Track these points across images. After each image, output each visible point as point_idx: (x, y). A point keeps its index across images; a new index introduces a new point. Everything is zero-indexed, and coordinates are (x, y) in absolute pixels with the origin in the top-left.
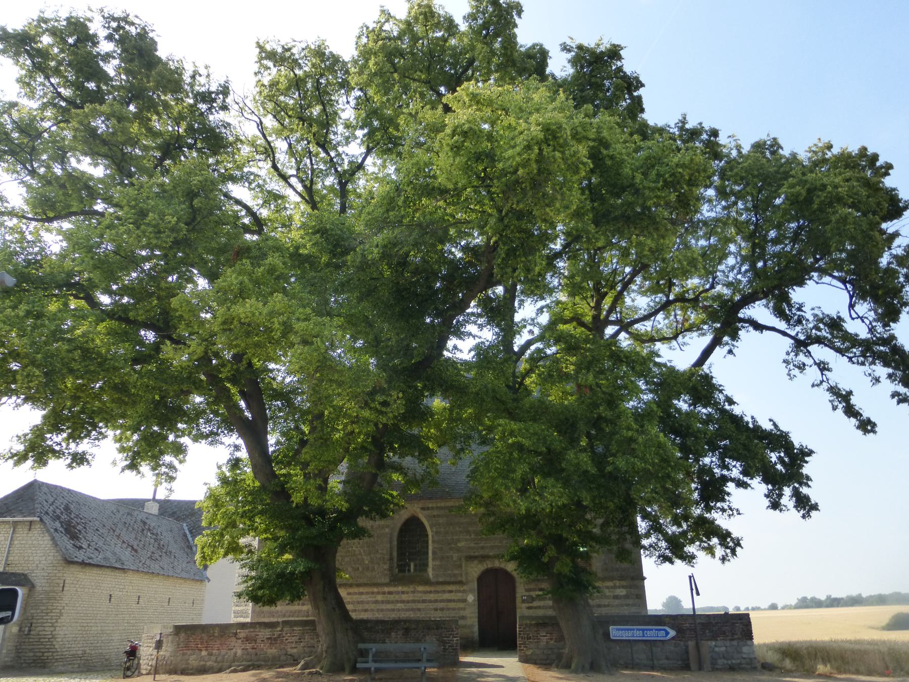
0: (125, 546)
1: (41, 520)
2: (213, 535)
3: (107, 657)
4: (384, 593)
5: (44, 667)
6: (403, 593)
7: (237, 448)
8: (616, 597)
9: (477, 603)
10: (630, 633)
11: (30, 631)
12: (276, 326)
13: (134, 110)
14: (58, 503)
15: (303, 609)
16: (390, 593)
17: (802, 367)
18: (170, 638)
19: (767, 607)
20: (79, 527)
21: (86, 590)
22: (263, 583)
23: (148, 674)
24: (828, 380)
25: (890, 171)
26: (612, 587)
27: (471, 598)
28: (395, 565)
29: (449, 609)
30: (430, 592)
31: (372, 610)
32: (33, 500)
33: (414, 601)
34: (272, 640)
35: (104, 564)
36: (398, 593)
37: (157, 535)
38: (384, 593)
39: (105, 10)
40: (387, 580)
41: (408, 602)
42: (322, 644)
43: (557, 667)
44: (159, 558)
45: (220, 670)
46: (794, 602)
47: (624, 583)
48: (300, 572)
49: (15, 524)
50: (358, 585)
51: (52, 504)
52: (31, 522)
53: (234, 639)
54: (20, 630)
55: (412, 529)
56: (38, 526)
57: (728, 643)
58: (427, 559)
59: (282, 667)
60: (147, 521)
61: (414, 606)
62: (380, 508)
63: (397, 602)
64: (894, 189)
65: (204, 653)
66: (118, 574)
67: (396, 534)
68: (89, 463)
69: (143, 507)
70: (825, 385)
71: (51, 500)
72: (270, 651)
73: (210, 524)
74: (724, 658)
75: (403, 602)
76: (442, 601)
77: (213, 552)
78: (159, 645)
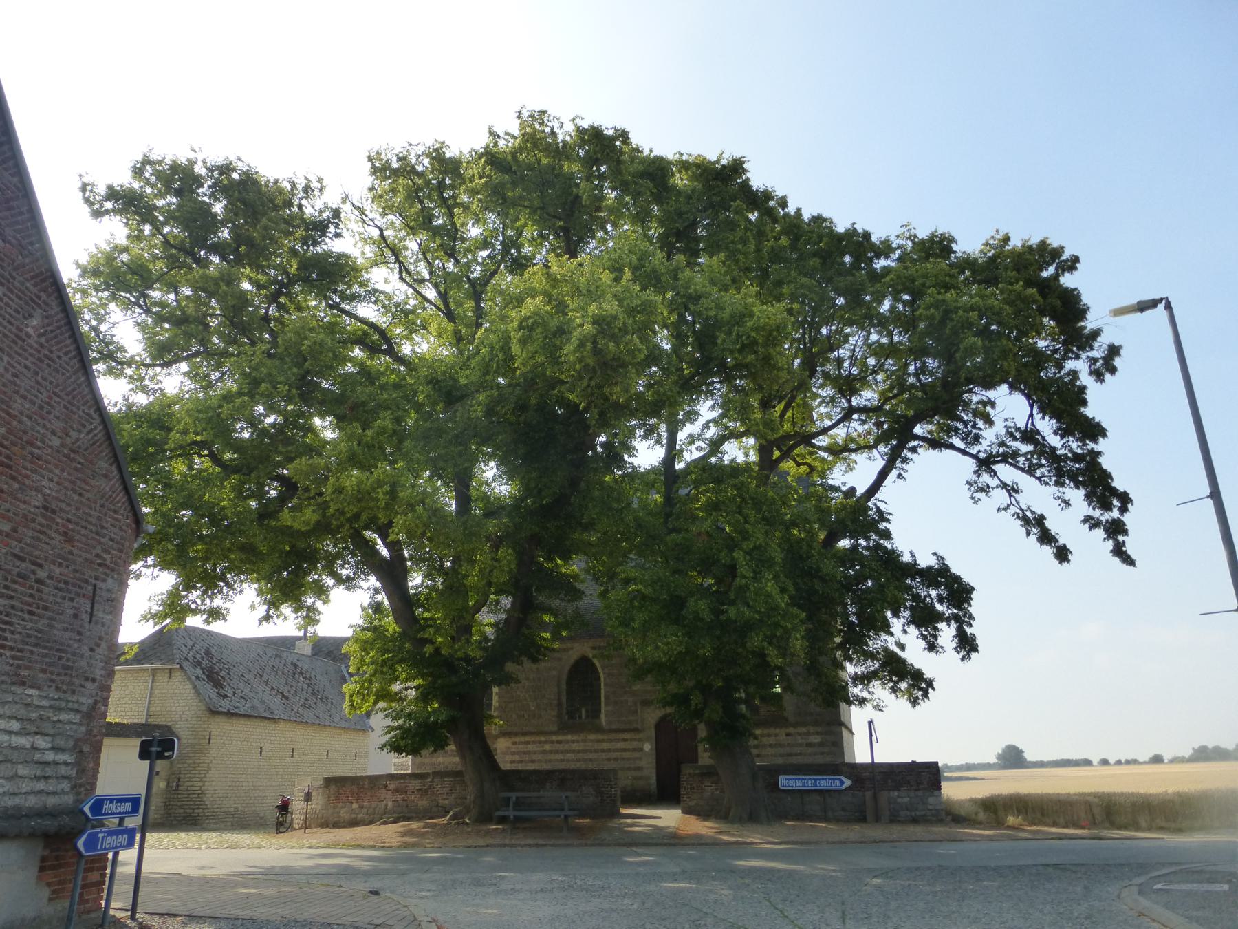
1: (181, 667)
2: (363, 682)
3: (262, 815)
4: (552, 742)
5: (196, 825)
6: (573, 742)
7: (377, 591)
8: (810, 745)
9: (654, 752)
11: (178, 786)
12: (381, 496)
13: (226, 458)
14: (197, 647)
15: (448, 758)
16: (559, 742)
17: (985, 489)
18: (321, 790)
19: (1147, 759)
22: (404, 733)
23: (300, 829)
24: (1017, 502)
25: (1078, 265)
26: (805, 734)
27: (647, 747)
28: (565, 711)
29: (623, 759)
30: (603, 741)
31: (540, 761)
32: (170, 645)
33: (585, 751)
34: (423, 792)
35: (252, 713)
36: (567, 742)
37: (310, 679)
38: (552, 742)
39: (207, 160)
40: (555, 728)
41: (579, 752)
42: (471, 794)
43: (716, 818)
44: (313, 706)
45: (370, 823)
46: (1187, 753)
47: (819, 729)
48: (443, 722)
49: (154, 672)
50: (524, 734)
51: (192, 648)
52: (170, 669)
53: (384, 791)
54: (168, 786)
55: (582, 674)
57: (912, 794)
58: (600, 704)
59: (432, 818)
60: (298, 663)
61: (585, 756)
62: (534, 652)
63: (567, 751)
64: (1076, 289)
65: (355, 806)
66: (266, 724)
67: (565, 677)
68: (224, 618)
69: (294, 645)
70: (1013, 509)
71: (190, 644)
72: (420, 803)
73: (359, 670)
74: (907, 809)
75: (573, 751)
77: (362, 700)
78: (308, 797)
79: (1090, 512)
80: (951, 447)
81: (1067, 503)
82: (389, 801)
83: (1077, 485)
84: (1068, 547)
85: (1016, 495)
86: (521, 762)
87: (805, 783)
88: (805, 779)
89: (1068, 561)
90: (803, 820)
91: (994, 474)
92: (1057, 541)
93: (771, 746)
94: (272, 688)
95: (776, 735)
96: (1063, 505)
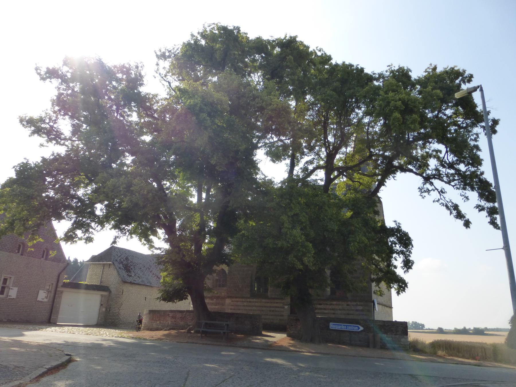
0: (153, 276)
4: (247, 302)
6: (256, 302)
8: (357, 310)
10: (340, 327)
11: (110, 310)
16: (250, 302)
17: (428, 191)
20: (132, 267)
21: (133, 294)
24: (444, 198)
25: (472, 79)
29: (276, 311)
30: (268, 302)
34: (182, 318)
36: (253, 302)
38: (247, 302)
47: (362, 303)
49: (104, 265)
50: (236, 297)
53: (168, 317)
56: (112, 266)
65: (158, 322)
71: (119, 255)
75: (256, 306)
76: (273, 307)
79: (479, 203)
80: (411, 171)
81: (467, 198)
82: (169, 321)
83: (473, 189)
84: (470, 220)
85: (443, 194)
86: (234, 309)
87: (341, 327)
88: (341, 325)
89: (469, 227)
90: (339, 343)
91: (432, 184)
92: (464, 217)
93: (340, 310)
94: (153, 274)
95: (342, 305)
96: (465, 199)
